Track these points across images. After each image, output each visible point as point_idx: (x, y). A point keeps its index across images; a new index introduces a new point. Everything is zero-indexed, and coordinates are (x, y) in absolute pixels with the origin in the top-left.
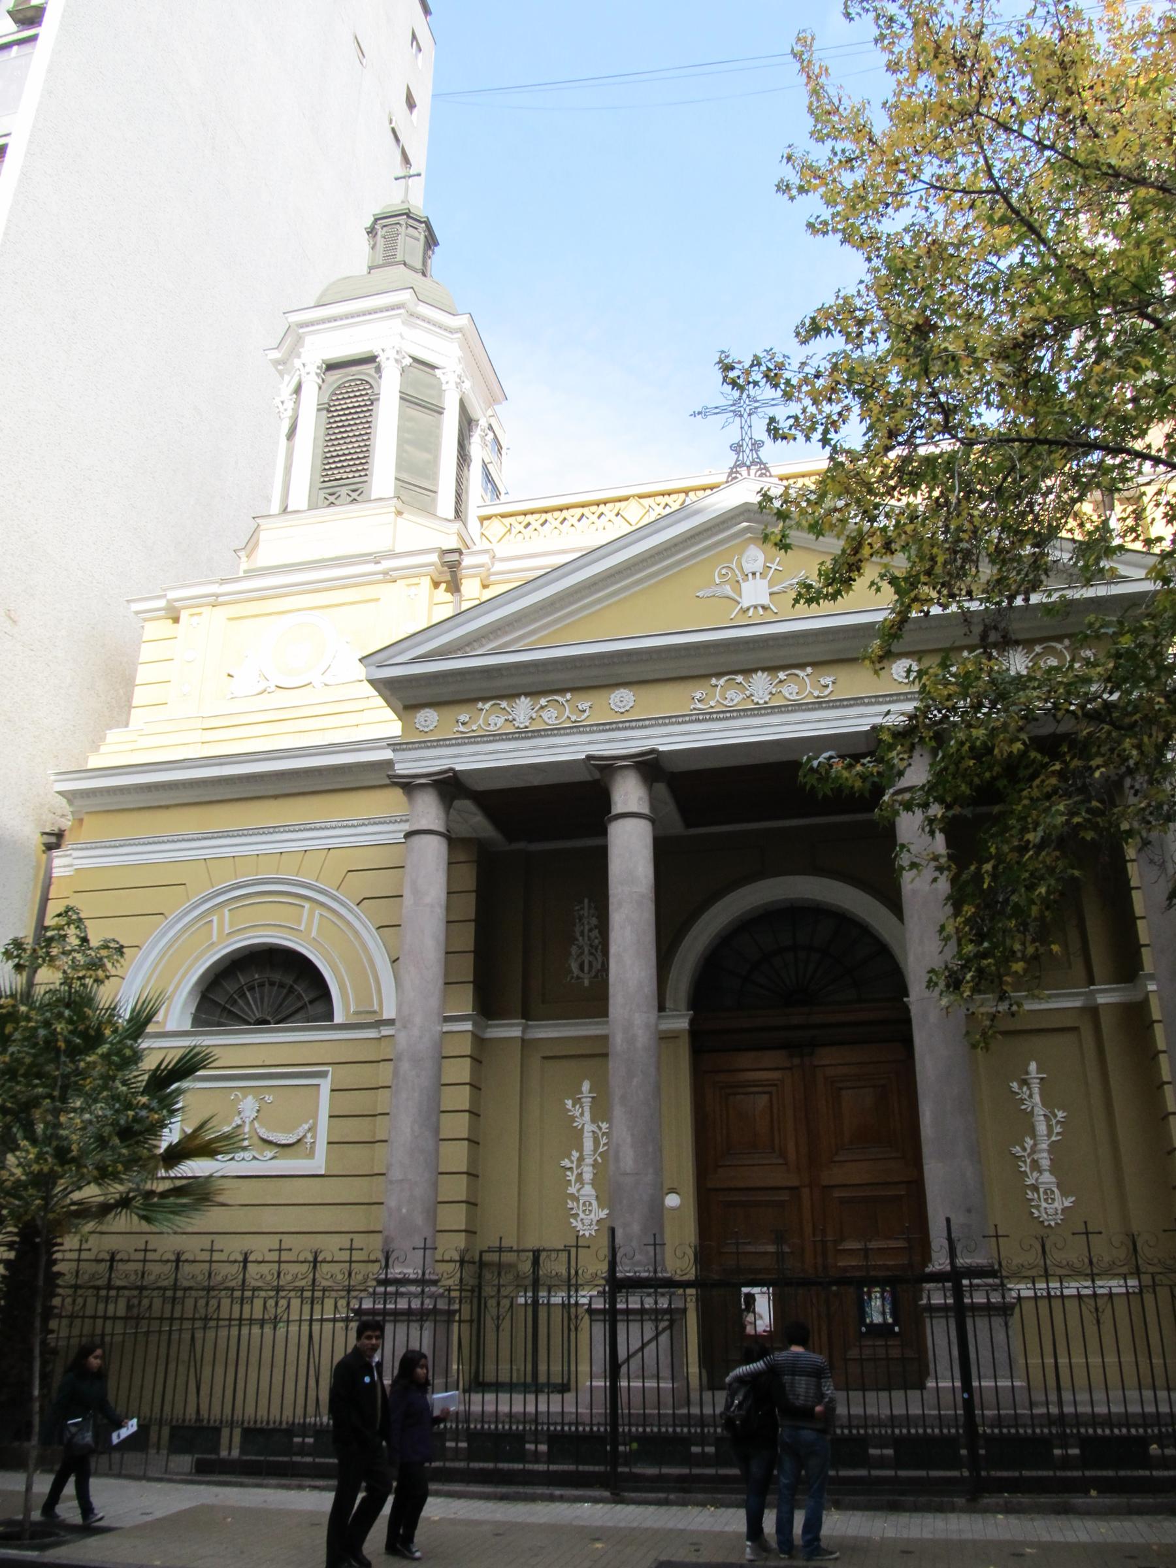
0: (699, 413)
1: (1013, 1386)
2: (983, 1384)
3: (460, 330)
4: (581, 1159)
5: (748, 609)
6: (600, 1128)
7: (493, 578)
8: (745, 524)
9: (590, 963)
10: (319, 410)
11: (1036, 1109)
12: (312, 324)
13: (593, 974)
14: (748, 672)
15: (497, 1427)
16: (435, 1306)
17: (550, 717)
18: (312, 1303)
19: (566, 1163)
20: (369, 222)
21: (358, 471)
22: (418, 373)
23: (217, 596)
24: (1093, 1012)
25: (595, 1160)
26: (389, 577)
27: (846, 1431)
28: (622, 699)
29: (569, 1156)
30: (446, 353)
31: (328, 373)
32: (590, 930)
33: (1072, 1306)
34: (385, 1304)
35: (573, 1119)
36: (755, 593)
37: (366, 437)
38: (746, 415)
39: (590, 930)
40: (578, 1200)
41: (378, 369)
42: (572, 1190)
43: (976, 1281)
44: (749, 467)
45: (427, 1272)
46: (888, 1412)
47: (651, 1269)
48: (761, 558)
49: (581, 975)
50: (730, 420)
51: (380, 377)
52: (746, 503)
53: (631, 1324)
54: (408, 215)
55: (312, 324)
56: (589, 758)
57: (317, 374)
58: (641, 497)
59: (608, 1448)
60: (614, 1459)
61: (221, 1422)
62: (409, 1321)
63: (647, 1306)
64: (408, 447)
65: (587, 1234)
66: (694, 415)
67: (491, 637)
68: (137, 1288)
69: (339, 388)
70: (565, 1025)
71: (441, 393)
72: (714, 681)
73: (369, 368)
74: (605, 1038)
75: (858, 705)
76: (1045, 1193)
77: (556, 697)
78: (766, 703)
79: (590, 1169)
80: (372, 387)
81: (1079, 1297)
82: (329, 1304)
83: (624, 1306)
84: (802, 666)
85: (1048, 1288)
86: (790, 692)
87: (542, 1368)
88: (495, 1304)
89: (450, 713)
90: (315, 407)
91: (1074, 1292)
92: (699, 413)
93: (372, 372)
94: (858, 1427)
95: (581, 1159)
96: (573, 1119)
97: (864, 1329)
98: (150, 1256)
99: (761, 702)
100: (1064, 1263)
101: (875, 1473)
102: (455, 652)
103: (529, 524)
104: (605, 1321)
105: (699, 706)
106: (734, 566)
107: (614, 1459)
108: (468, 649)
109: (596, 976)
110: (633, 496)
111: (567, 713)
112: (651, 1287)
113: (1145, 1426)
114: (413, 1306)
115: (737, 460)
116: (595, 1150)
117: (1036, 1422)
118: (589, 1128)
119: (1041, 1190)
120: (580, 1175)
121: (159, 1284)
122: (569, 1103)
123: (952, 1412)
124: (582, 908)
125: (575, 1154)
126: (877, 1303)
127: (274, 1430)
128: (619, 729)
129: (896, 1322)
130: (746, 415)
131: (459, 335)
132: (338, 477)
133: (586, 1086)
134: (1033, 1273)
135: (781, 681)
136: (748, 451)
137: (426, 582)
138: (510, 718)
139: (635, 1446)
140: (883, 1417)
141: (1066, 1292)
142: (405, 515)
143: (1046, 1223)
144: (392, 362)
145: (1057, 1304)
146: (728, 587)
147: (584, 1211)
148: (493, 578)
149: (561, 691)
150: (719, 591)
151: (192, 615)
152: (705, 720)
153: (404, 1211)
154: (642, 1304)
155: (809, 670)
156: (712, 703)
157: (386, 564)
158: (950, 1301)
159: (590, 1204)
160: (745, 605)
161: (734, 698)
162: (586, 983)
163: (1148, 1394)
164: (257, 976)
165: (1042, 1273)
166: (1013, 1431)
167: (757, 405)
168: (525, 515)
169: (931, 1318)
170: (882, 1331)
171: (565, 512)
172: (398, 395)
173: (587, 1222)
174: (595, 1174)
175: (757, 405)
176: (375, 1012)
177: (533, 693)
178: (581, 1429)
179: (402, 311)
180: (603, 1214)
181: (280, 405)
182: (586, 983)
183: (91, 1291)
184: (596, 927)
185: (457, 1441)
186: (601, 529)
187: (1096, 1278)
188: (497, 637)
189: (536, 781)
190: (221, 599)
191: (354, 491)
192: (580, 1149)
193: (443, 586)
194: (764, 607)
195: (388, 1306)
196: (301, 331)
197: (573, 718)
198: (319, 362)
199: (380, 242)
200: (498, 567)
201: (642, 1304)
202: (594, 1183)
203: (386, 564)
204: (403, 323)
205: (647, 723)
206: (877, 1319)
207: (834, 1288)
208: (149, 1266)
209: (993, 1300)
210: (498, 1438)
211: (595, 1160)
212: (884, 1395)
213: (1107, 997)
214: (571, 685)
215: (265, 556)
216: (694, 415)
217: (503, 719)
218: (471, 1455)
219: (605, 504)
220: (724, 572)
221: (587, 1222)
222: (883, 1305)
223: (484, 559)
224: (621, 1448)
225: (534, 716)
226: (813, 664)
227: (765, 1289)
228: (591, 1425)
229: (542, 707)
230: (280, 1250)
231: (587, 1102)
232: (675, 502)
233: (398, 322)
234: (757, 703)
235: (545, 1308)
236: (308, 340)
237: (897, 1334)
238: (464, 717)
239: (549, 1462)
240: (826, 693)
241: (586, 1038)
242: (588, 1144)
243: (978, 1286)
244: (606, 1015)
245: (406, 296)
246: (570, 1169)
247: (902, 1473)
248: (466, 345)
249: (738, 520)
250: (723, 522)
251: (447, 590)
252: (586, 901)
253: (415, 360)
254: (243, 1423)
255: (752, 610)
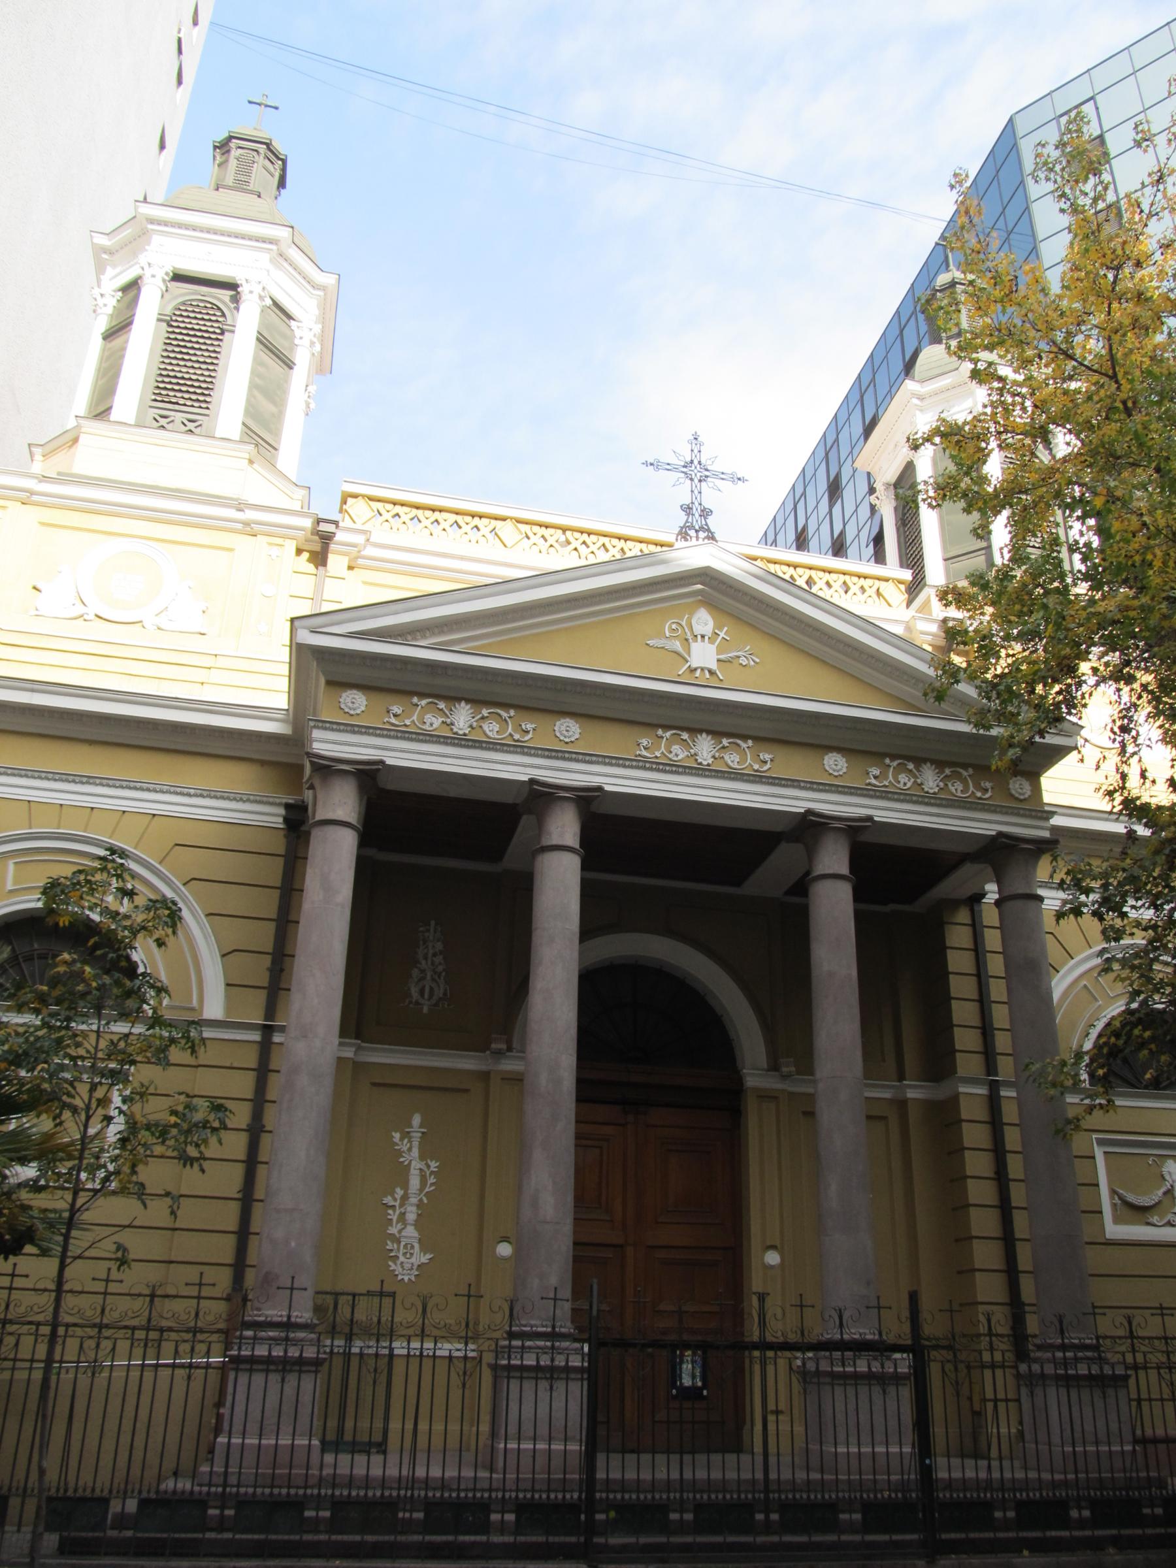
0: (652, 464)
1: (901, 1453)
2: (522, 1446)
3: (323, 288)
4: (405, 1198)
5: (696, 669)
6: (428, 1166)
7: (360, 561)
8: (699, 586)
9: (431, 989)
10: (159, 320)
11: (413, 1163)
12: (166, 224)
13: (434, 1001)
14: (694, 731)
15: (739, 1497)
16: (817, 1368)
17: (492, 729)
18: (146, 1345)
19: (388, 1200)
20: (222, 136)
21: (198, 400)
22: (275, 318)
23: (32, 493)
24: (902, 1104)
25: (421, 1200)
26: (249, 529)
27: (470, 1495)
28: (568, 729)
29: (392, 1194)
30: (305, 308)
31: (174, 283)
32: (434, 955)
33: (441, 1368)
34: (509, 1358)
35: (400, 1153)
36: (704, 655)
37: (212, 363)
38: (696, 481)
39: (434, 955)
40: (399, 1242)
41: (236, 299)
42: (393, 1230)
43: (528, 1343)
44: (697, 531)
45: (558, 1324)
46: (364, 1472)
47: (549, 1324)
48: (711, 624)
49: (421, 1001)
50: (682, 480)
51: (237, 309)
52: (708, 567)
53: (240, 1374)
54: (268, 145)
55: (166, 224)
56: (532, 781)
57: (164, 281)
58: (519, 521)
59: (583, 1517)
60: (591, 1528)
61: (10, 1489)
62: (267, 1371)
63: (542, 1363)
64: (256, 393)
65: (406, 1278)
66: (646, 464)
67: (436, 630)
68: (94, 1326)
69: (184, 304)
70: (384, 1050)
71: (293, 346)
72: (415, 700)
73: (225, 295)
74: (811, 1098)
75: (794, 787)
76: (405, 1246)
77: (499, 711)
78: (465, 735)
79: (414, 1209)
80: (224, 315)
81: (450, 1358)
82: (168, 1347)
83: (519, 1362)
84: (744, 738)
85: (332, 1346)
86: (732, 760)
87: (349, 1424)
88: (952, 1368)
89: (382, 700)
90: (156, 316)
91: (446, 1353)
92: (652, 464)
93: (227, 299)
94: (747, 1492)
95: (405, 1198)
96: (400, 1153)
97: (674, 1391)
98: (19, 1282)
99: (705, 763)
100: (76, 1310)
101: (844, 1538)
102: (396, 637)
103: (397, 515)
104: (582, 1379)
105: (644, 753)
106: (684, 623)
107: (591, 1528)
108: (409, 637)
109: (436, 1005)
110: (511, 519)
111: (510, 730)
112: (877, 1350)
113: (623, 1491)
114: (1093, 1372)
115: (687, 521)
116: (421, 1190)
117: (416, 1485)
118: (416, 1165)
119: (403, 1244)
120: (403, 1214)
121: (30, 1319)
122: (397, 1136)
123: (871, 1477)
124: (428, 931)
125: (399, 1192)
126: (687, 1367)
127: (83, 1500)
128: (564, 759)
129: (704, 1386)
130: (696, 481)
131: (321, 293)
132: (174, 400)
133: (416, 1120)
134: (410, 1332)
135: (723, 747)
136: (697, 515)
137: (291, 546)
138: (448, 721)
139: (612, 1514)
140: (798, 1481)
141: (438, 1353)
142: (255, 466)
143: (400, 1277)
144: (255, 297)
145: (427, 1364)
146: (678, 643)
147: (405, 1254)
148: (360, 561)
149: (506, 706)
150: (669, 645)
151: (270, 544)
152: (651, 769)
153: (293, 1244)
154: (538, 1362)
155: (971, 771)
156: (658, 754)
157: (250, 515)
158: (586, 1364)
159: (412, 1247)
160: (694, 665)
161: (679, 753)
162: (425, 1010)
163: (1006, 1464)
164: (36, 946)
165: (418, 1332)
166: (529, 1495)
167: (707, 473)
168: (395, 504)
169: (508, 1378)
170: (692, 1394)
171: (437, 513)
172: (255, 334)
173: (407, 1266)
174: (419, 1215)
175: (707, 473)
176: (193, 1009)
177: (476, 701)
178: (537, 1496)
179: (274, 247)
180: (425, 1259)
181: (99, 297)
182: (425, 1010)
183: (27, 1327)
184: (441, 953)
185: (682, 1512)
186: (474, 541)
187: (470, 1341)
188: (442, 632)
189: (914, 842)
190: (35, 498)
191: (162, 417)
192: (405, 1186)
193: (306, 555)
194: (711, 672)
195: (513, 1362)
196: (150, 227)
197: (517, 737)
198: (169, 269)
199: (233, 163)
200: (370, 551)
201: (538, 1362)
202: (417, 1225)
203: (250, 515)
204: (271, 261)
205: (594, 758)
206: (687, 1381)
207: (650, 1350)
208: (15, 1295)
209: (874, 1369)
210: (459, 1506)
211: (421, 1200)
212: (675, 1458)
213: (915, 1092)
214: (516, 702)
215: (84, 460)
216: (646, 464)
217: (441, 720)
218: (334, 1525)
219: (626, 540)
220: (674, 626)
221: (407, 1266)
222: (693, 1368)
223: (359, 539)
224: (600, 1517)
225: (475, 724)
226: (756, 739)
227: (905, 1355)
228: (459, 1490)
229: (483, 718)
230: (200, 1285)
231: (416, 1136)
232: (634, 549)
233: (265, 257)
234: (701, 764)
235: (431, 1361)
236: (156, 239)
237: (705, 1398)
238: (396, 709)
239: (517, 1533)
240: (765, 768)
241: (408, 1067)
242: (414, 1182)
243: (530, 1348)
244: (812, 1073)
245: (283, 233)
246: (393, 1207)
247: (870, 1538)
248: (323, 307)
249: (695, 581)
250: (682, 578)
251: (310, 560)
252: (433, 923)
253: (276, 304)
254: (140, 1492)
255: (699, 671)
